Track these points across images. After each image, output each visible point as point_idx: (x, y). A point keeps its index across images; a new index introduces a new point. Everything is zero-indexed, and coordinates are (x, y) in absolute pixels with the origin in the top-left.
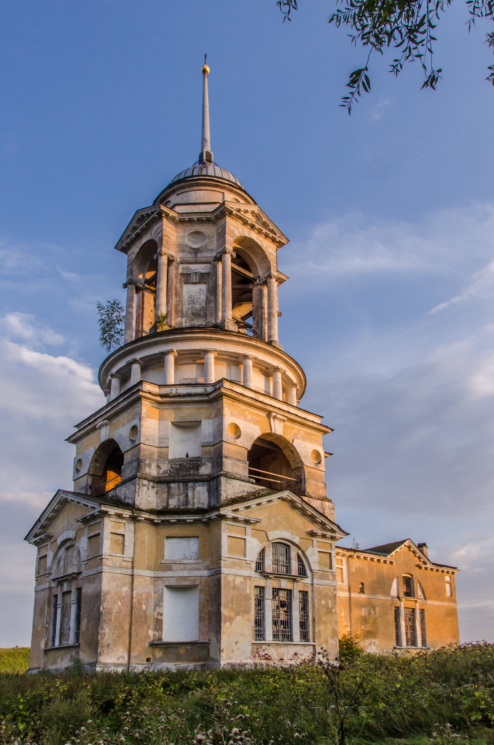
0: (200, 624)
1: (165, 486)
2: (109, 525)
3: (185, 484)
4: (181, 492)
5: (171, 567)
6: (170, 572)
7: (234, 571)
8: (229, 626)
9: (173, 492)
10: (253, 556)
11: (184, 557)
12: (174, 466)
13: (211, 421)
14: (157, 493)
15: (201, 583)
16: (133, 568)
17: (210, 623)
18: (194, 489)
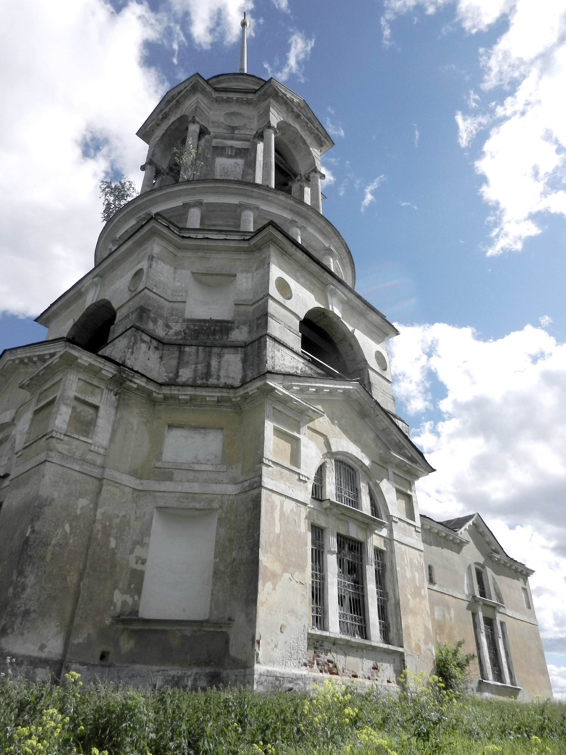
0: (214, 584)
1: (176, 348)
2: (72, 385)
3: (207, 349)
4: (200, 359)
5: (172, 474)
6: (168, 483)
7: (281, 487)
8: (270, 591)
9: (186, 358)
10: (309, 469)
11: (195, 461)
12: (192, 327)
14: (161, 358)
15: (221, 507)
16: (103, 467)
17: (234, 583)
18: (220, 356)
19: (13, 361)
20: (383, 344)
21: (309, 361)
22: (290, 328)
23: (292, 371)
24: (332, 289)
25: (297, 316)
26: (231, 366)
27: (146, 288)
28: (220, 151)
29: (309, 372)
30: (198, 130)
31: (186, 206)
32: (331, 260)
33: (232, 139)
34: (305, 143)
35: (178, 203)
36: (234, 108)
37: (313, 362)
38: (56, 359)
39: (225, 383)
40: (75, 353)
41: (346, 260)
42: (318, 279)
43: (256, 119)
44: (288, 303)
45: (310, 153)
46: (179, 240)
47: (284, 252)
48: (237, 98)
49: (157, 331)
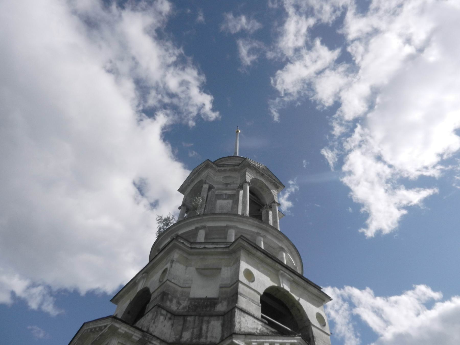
3: (201, 318)
12: (193, 303)
13: (229, 268)
14: (172, 325)
18: (208, 322)
19: (87, 330)
20: (322, 307)
21: (265, 323)
22: (253, 301)
23: (253, 331)
24: (282, 274)
25: (258, 293)
26: (215, 328)
27: (167, 280)
28: (219, 197)
29: (266, 331)
30: (208, 187)
31: (197, 229)
32: (284, 254)
33: (226, 190)
34: (268, 188)
35: (193, 227)
36: (228, 174)
37: (270, 324)
38: (106, 330)
39: (211, 341)
40: (117, 325)
41: (295, 253)
42: (272, 267)
43: (239, 178)
44: (252, 285)
45: (271, 193)
46: (190, 250)
47: (249, 253)
48: (229, 169)
49: (172, 307)
